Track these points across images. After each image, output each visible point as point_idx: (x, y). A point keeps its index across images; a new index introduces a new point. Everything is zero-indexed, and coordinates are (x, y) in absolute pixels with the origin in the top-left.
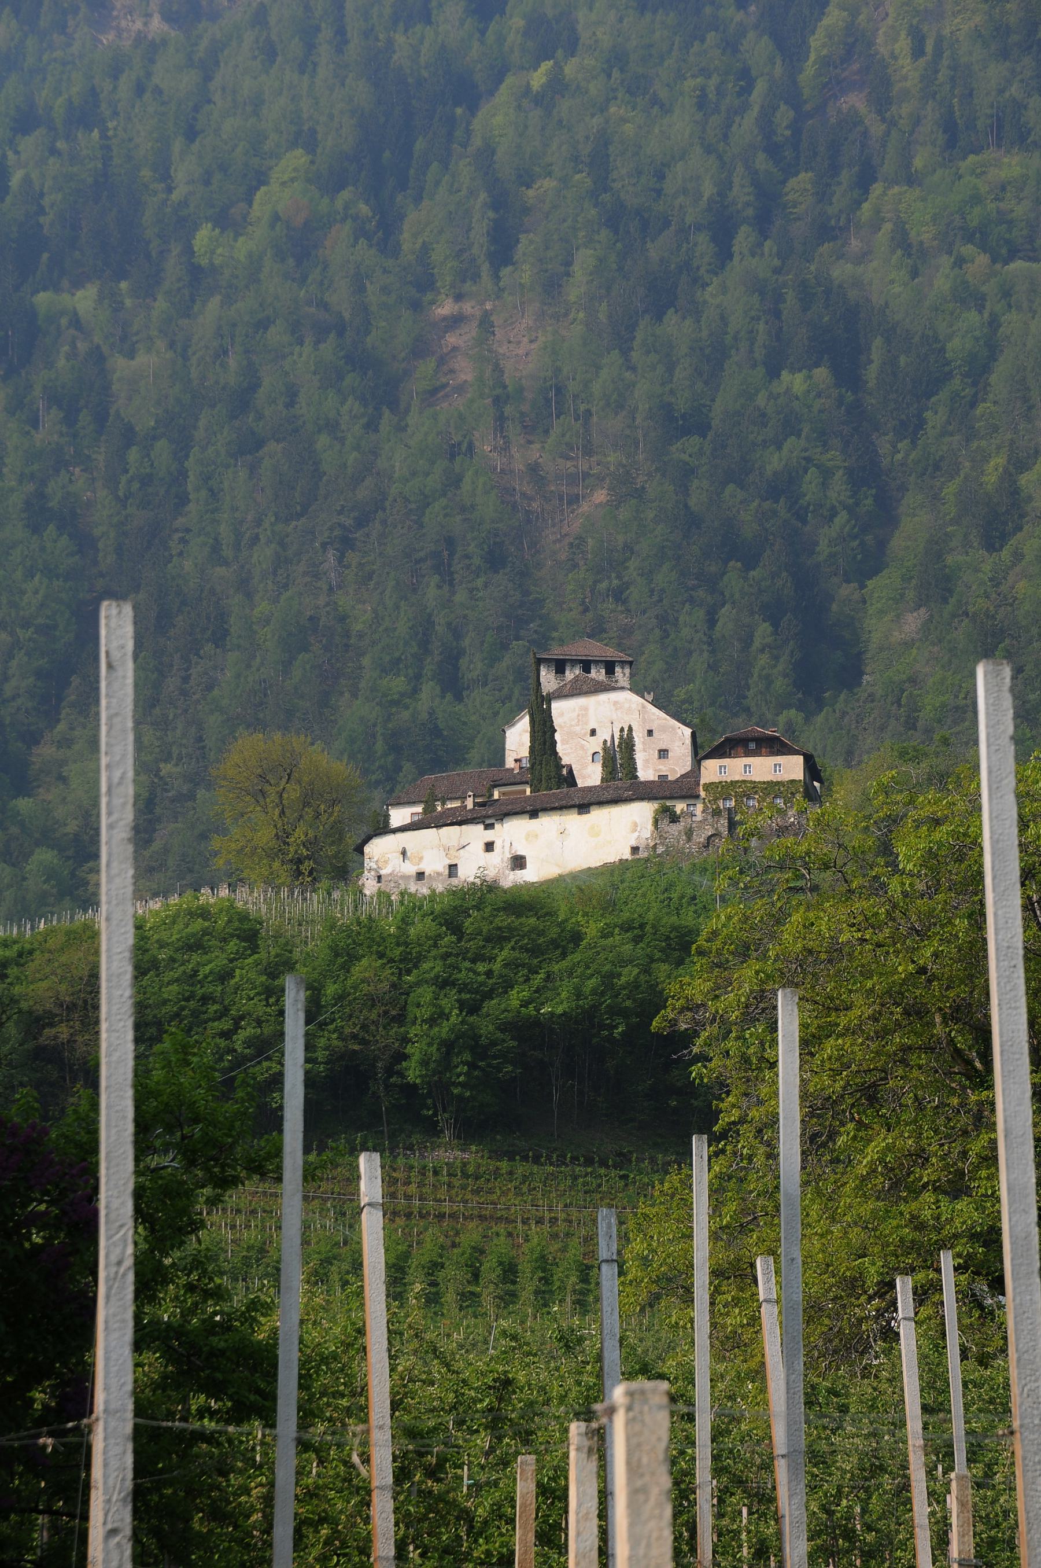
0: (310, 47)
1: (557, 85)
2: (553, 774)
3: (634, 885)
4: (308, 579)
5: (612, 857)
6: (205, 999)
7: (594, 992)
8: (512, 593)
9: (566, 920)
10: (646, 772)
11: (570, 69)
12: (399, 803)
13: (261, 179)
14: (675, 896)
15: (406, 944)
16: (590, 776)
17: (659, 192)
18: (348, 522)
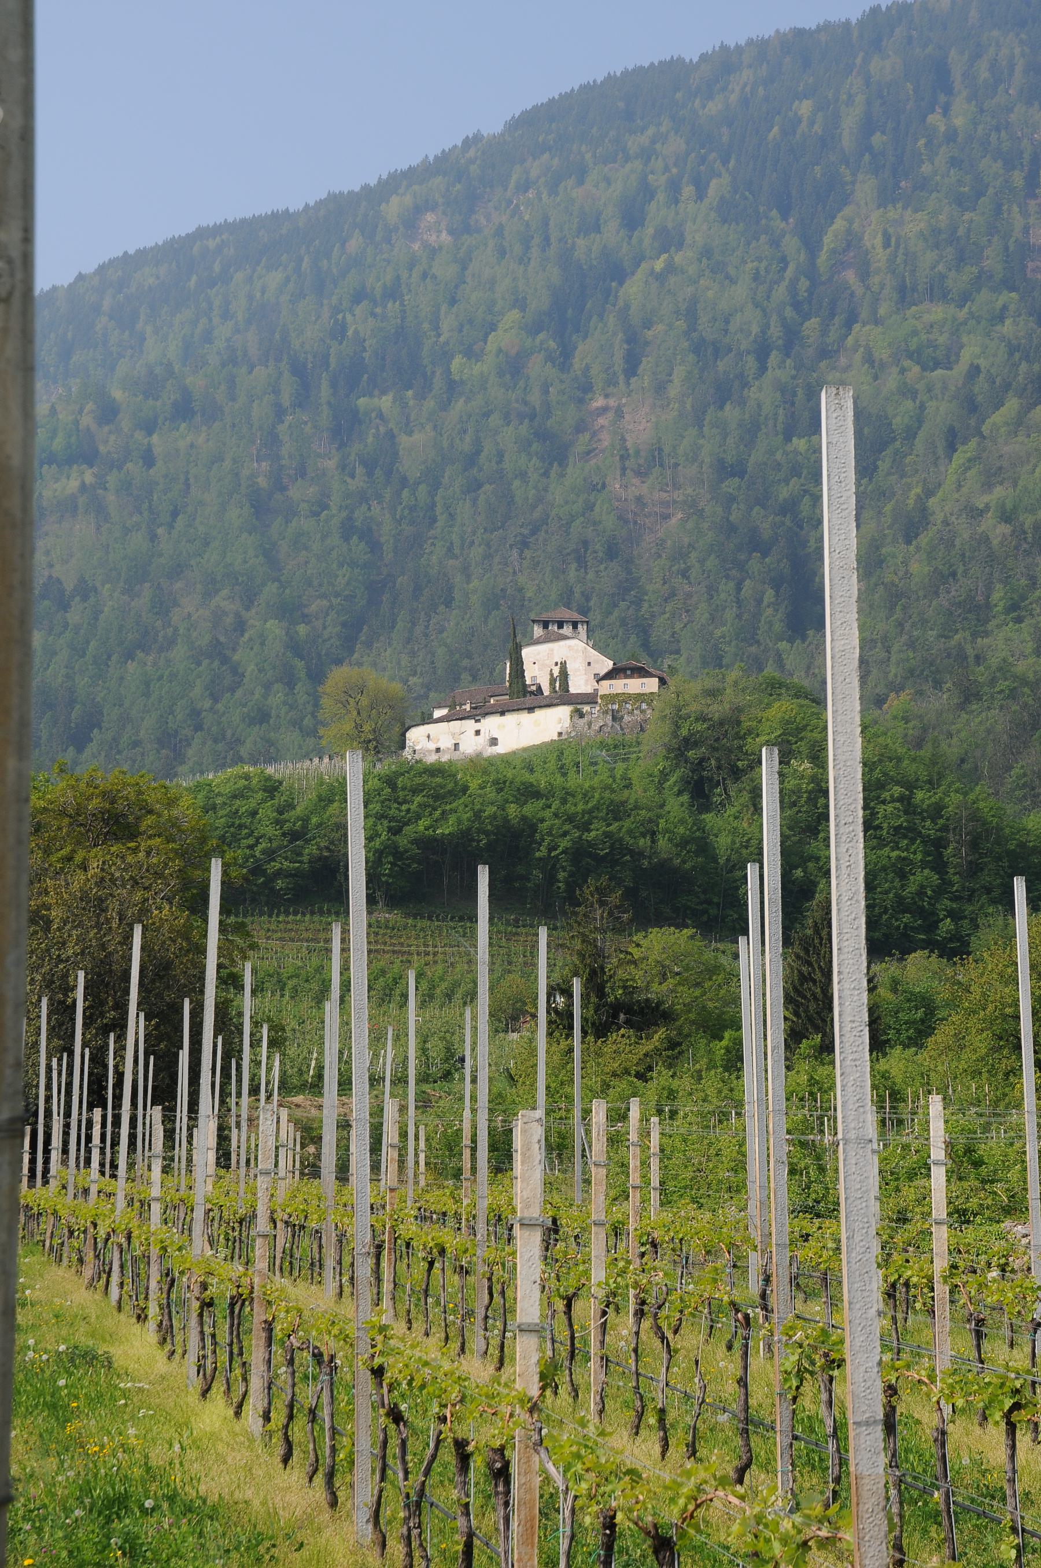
0: (528, 248)
1: (670, 268)
5: (547, 739)
6: (241, 827)
7: (469, 820)
11: (678, 258)
13: (493, 327)
17: (726, 331)
18: (526, 532)
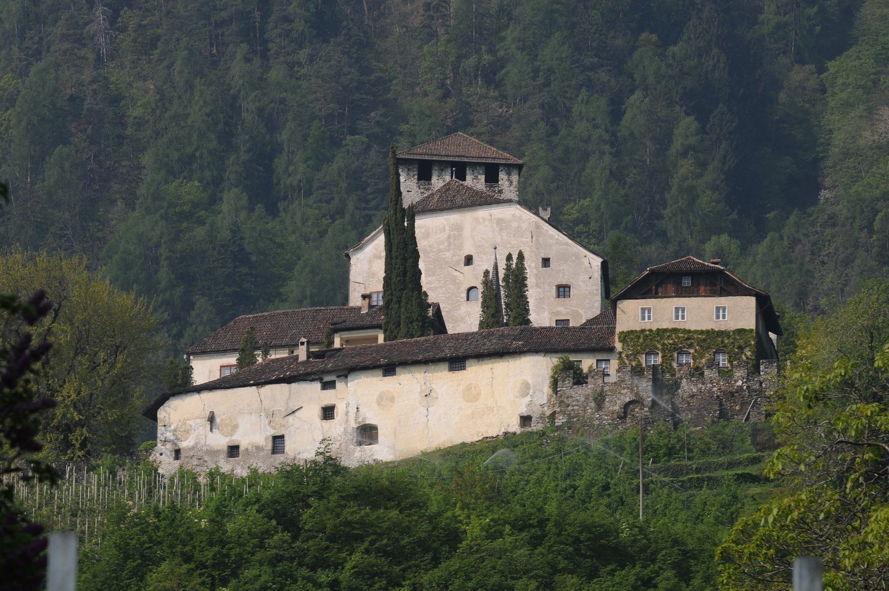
2: (415, 316)
3: (524, 467)
4: (66, 45)
8: (346, 70)
9: (440, 514)
10: (541, 315)
12: (204, 352)
14: (581, 483)
15: (223, 543)
16: (464, 318)
